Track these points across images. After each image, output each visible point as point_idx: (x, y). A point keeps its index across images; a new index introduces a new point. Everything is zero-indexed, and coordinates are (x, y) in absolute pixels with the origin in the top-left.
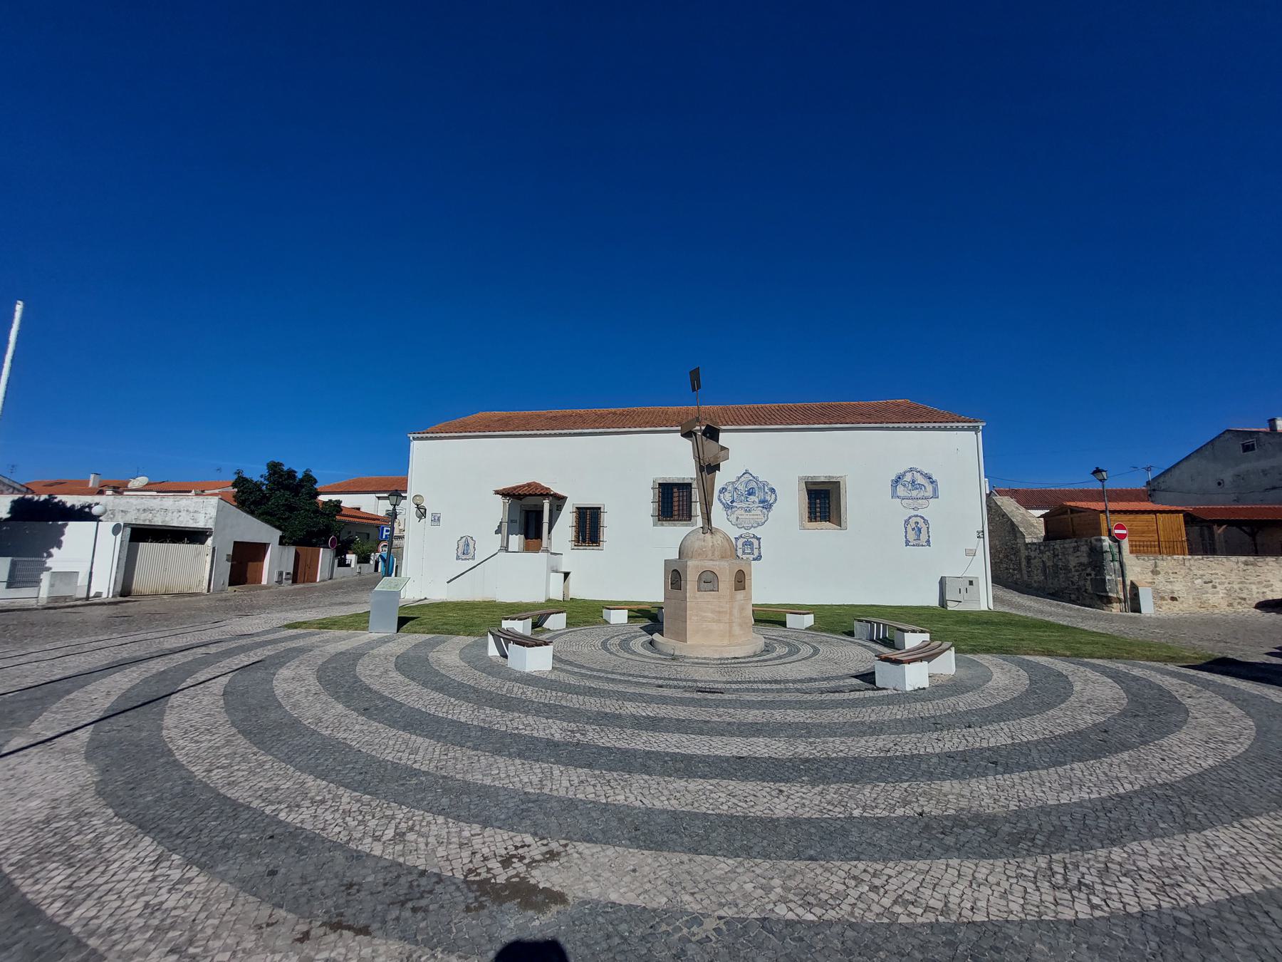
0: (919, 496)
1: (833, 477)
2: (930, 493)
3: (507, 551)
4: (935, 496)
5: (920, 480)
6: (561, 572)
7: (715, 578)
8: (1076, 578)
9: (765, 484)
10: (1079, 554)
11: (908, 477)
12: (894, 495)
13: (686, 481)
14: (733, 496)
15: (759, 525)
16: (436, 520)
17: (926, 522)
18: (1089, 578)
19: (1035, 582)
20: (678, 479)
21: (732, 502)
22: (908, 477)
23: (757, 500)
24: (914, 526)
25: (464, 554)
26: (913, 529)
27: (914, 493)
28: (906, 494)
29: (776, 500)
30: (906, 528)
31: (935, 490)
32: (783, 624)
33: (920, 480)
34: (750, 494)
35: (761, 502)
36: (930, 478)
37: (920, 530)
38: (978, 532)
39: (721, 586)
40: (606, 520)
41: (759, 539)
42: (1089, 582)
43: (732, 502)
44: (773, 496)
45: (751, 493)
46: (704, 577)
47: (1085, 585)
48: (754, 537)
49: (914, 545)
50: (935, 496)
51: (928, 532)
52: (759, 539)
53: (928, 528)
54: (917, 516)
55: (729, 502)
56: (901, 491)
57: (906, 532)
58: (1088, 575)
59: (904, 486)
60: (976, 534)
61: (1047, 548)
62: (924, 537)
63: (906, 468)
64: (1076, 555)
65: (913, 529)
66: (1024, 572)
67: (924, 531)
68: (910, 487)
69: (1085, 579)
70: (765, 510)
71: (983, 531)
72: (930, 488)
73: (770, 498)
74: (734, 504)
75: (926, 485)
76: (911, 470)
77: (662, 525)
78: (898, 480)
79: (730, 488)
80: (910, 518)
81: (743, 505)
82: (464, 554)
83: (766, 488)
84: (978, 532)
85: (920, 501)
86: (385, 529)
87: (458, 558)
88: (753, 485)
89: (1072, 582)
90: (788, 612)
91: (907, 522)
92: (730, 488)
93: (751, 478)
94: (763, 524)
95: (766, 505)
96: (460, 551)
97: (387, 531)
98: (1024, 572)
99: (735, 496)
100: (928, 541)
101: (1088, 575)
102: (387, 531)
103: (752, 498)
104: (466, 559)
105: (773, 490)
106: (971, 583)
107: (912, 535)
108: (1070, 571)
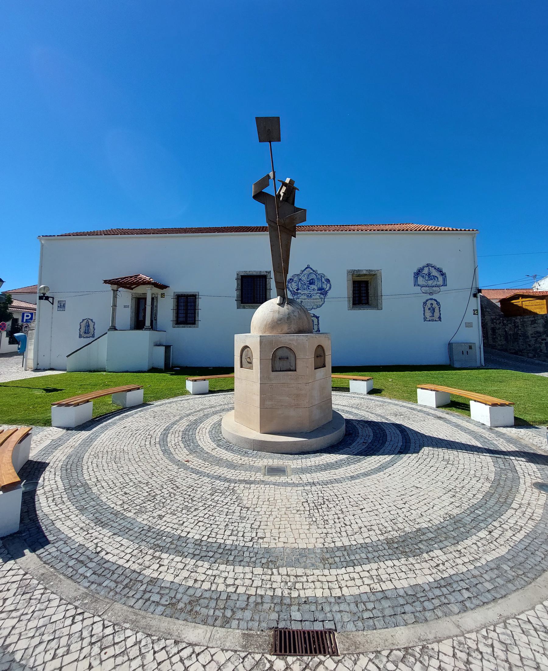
0: (433, 284)
1: (372, 271)
2: (441, 282)
3: (115, 329)
4: (445, 285)
5: (434, 273)
6: (164, 346)
7: (292, 355)
8: (533, 342)
9: (322, 276)
10: (536, 325)
11: (426, 271)
12: (416, 284)
13: (262, 274)
14: (298, 285)
15: (318, 307)
16: (62, 306)
17: (438, 303)
18: (544, 342)
19: (499, 345)
20: (257, 272)
21: (298, 290)
22: (426, 271)
23: (316, 288)
24: (429, 306)
25: (85, 333)
26: (429, 309)
27: (430, 282)
28: (424, 283)
29: (330, 288)
30: (424, 308)
31: (445, 280)
32: (347, 389)
33: (434, 273)
34: (311, 284)
35: (319, 289)
36: (441, 271)
37: (434, 310)
38: (474, 310)
39: (300, 365)
40: (201, 304)
41: (318, 318)
42: (544, 345)
43: (298, 290)
44: (328, 285)
45: (312, 282)
46: (280, 354)
47: (540, 347)
48: (314, 316)
49: (429, 321)
50: (445, 285)
51: (440, 311)
52: (318, 318)
53: (440, 308)
54: (432, 299)
55: (295, 290)
56: (421, 281)
57: (424, 311)
58: (543, 340)
59: (423, 277)
60: (473, 312)
61: (509, 322)
62: (437, 314)
63: (424, 263)
64: (533, 326)
65: (429, 309)
66: (490, 339)
67: (437, 310)
68: (427, 278)
69: (541, 343)
70: (322, 296)
71: (477, 310)
72: (441, 278)
73: (326, 287)
74: (299, 291)
75: (438, 276)
76: (428, 265)
77: (244, 308)
78: (418, 273)
79: (296, 279)
80: (427, 301)
81: (306, 292)
82: (85, 333)
83: (323, 279)
84: (474, 310)
85: (434, 288)
86: (25, 314)
87: (80, 336)
88: (314, 276)
89: (529, 345)
90: (351, 379)
91: (425, 303)
92: (296, 279)
93: (312, 271)
94: (321, 306)
95: (323, 292)
96: (83, 330)
97: (27, 316)
98: (490, 339)
99: (300, 285)
100: (440, 318)
101: (543, 340)
102: (27, 316)
103: (312, 287)
104: (87, 337)
105: (328, 281)
106: (470, 348)
107: (428, 314)
108: (528, 337)
